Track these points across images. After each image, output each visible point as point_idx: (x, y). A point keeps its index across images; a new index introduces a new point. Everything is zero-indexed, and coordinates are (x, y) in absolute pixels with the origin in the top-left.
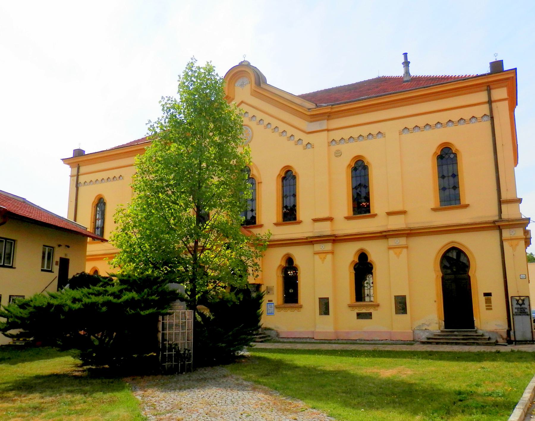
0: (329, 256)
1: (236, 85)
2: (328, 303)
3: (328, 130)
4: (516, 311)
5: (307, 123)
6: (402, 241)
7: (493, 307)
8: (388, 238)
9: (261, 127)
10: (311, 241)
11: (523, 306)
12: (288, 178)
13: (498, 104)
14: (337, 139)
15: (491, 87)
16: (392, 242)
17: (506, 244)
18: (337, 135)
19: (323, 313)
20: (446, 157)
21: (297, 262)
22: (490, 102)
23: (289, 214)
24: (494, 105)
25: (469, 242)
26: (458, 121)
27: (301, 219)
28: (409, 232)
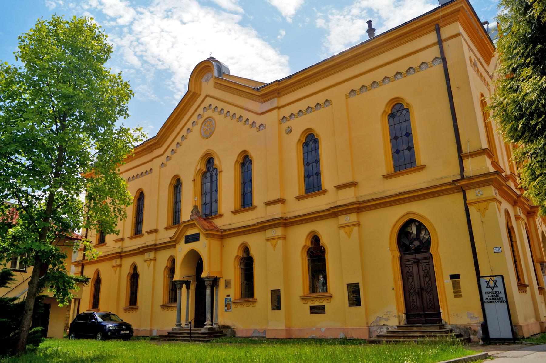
0: (280, 242)
1: (202, 81)
2: (280, 295)
3: (279, 108)
4: (487, 296)
5: (260, 104)
6: (352, 218)
7: (463, 293)
8: (337, 216)
9: (222, 116)
10: (333, 213)
11: (495, 289)
12: (245, 163)
13: (449, 42)
14: (287, 115)
15: (440, 25)
16: (343, 220)
17: (471, 209)
18: (286, 112)
19: (275, 308)
20: (398, 113)
21: (325, 241)
22: (440, 42)
23: (246, 201)
24: (445, 44)
25: (430, 212)
26: (407, 71)
27: (326, 188)
28: (358, 206)
